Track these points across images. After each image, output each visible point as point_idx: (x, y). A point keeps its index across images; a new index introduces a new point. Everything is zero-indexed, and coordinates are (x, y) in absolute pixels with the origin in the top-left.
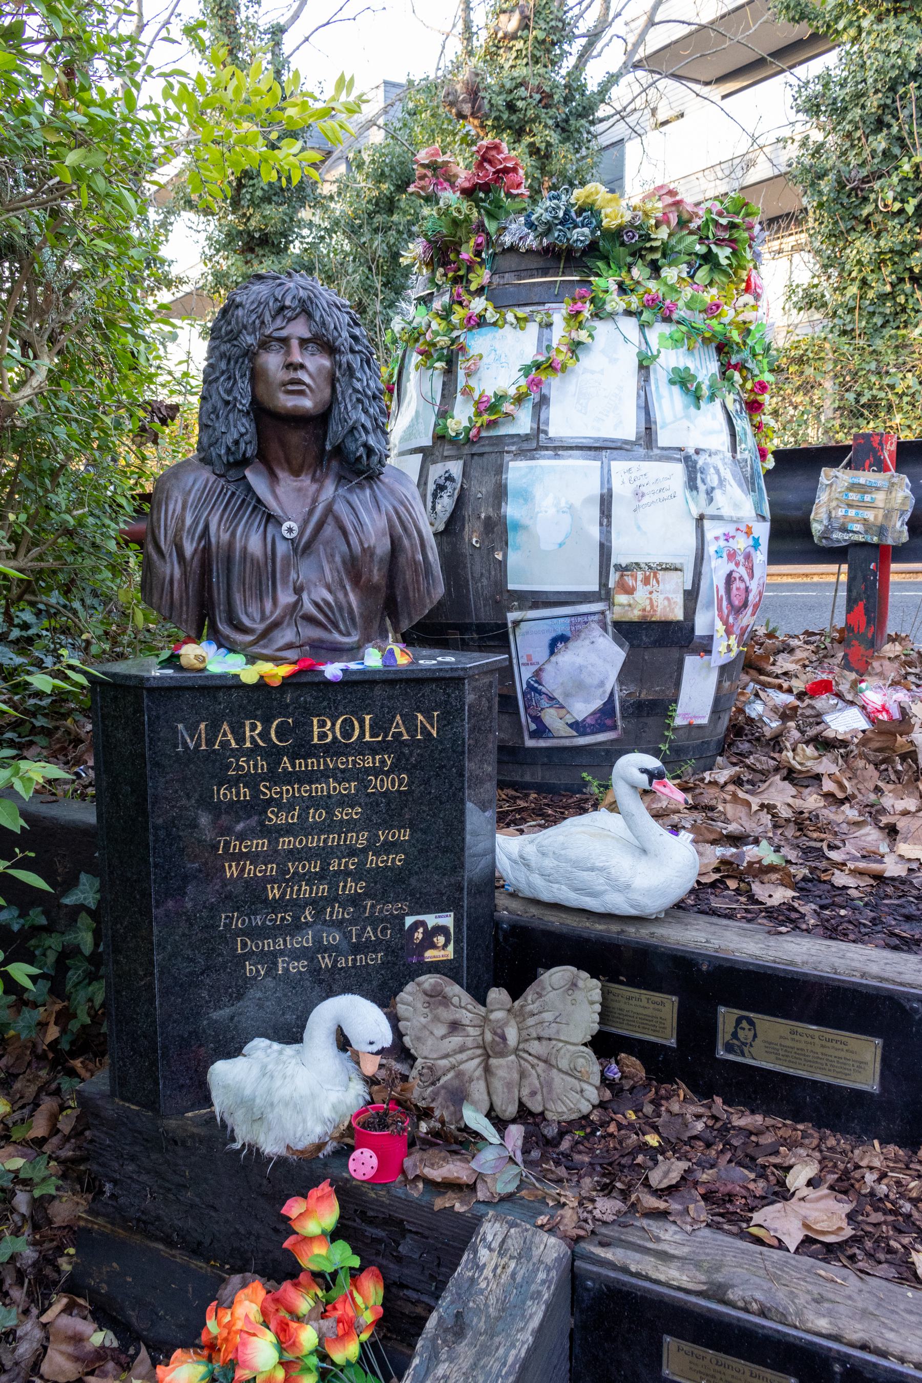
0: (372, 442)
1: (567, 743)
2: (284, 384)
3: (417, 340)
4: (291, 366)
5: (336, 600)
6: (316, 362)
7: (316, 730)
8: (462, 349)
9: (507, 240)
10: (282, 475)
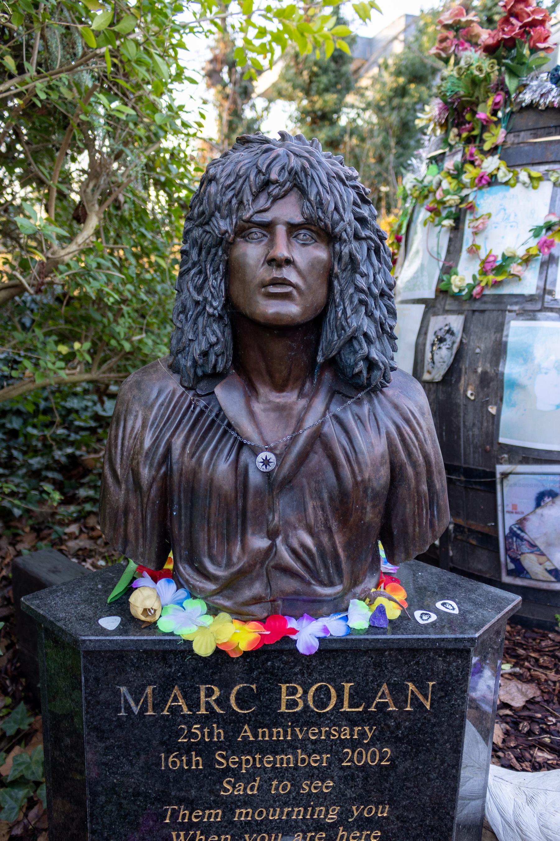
0: (375, 355)
1: (544, 586)
2: (264, 285)
3: (426, 197)
4: (274, 262)
5: (319, 545)
6: (309, 255)
7: (284, 697)
8: (471, 208)
9: (527, 97)
10: (263, 390)
